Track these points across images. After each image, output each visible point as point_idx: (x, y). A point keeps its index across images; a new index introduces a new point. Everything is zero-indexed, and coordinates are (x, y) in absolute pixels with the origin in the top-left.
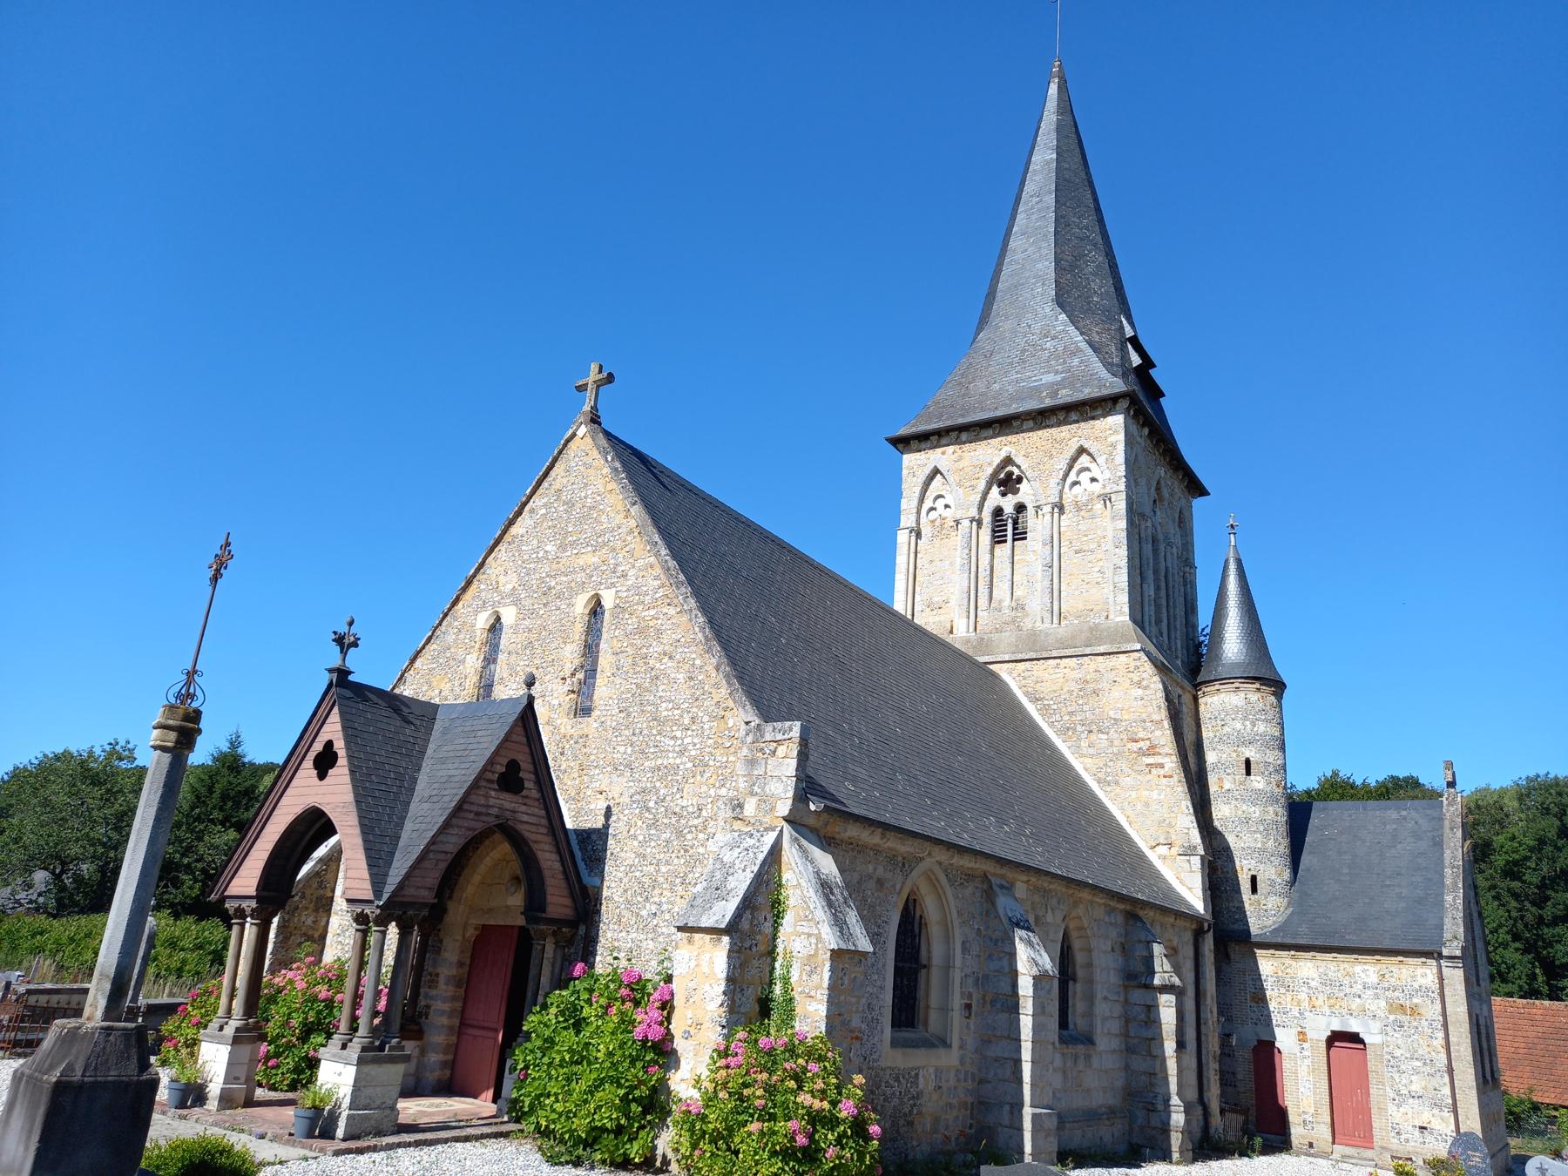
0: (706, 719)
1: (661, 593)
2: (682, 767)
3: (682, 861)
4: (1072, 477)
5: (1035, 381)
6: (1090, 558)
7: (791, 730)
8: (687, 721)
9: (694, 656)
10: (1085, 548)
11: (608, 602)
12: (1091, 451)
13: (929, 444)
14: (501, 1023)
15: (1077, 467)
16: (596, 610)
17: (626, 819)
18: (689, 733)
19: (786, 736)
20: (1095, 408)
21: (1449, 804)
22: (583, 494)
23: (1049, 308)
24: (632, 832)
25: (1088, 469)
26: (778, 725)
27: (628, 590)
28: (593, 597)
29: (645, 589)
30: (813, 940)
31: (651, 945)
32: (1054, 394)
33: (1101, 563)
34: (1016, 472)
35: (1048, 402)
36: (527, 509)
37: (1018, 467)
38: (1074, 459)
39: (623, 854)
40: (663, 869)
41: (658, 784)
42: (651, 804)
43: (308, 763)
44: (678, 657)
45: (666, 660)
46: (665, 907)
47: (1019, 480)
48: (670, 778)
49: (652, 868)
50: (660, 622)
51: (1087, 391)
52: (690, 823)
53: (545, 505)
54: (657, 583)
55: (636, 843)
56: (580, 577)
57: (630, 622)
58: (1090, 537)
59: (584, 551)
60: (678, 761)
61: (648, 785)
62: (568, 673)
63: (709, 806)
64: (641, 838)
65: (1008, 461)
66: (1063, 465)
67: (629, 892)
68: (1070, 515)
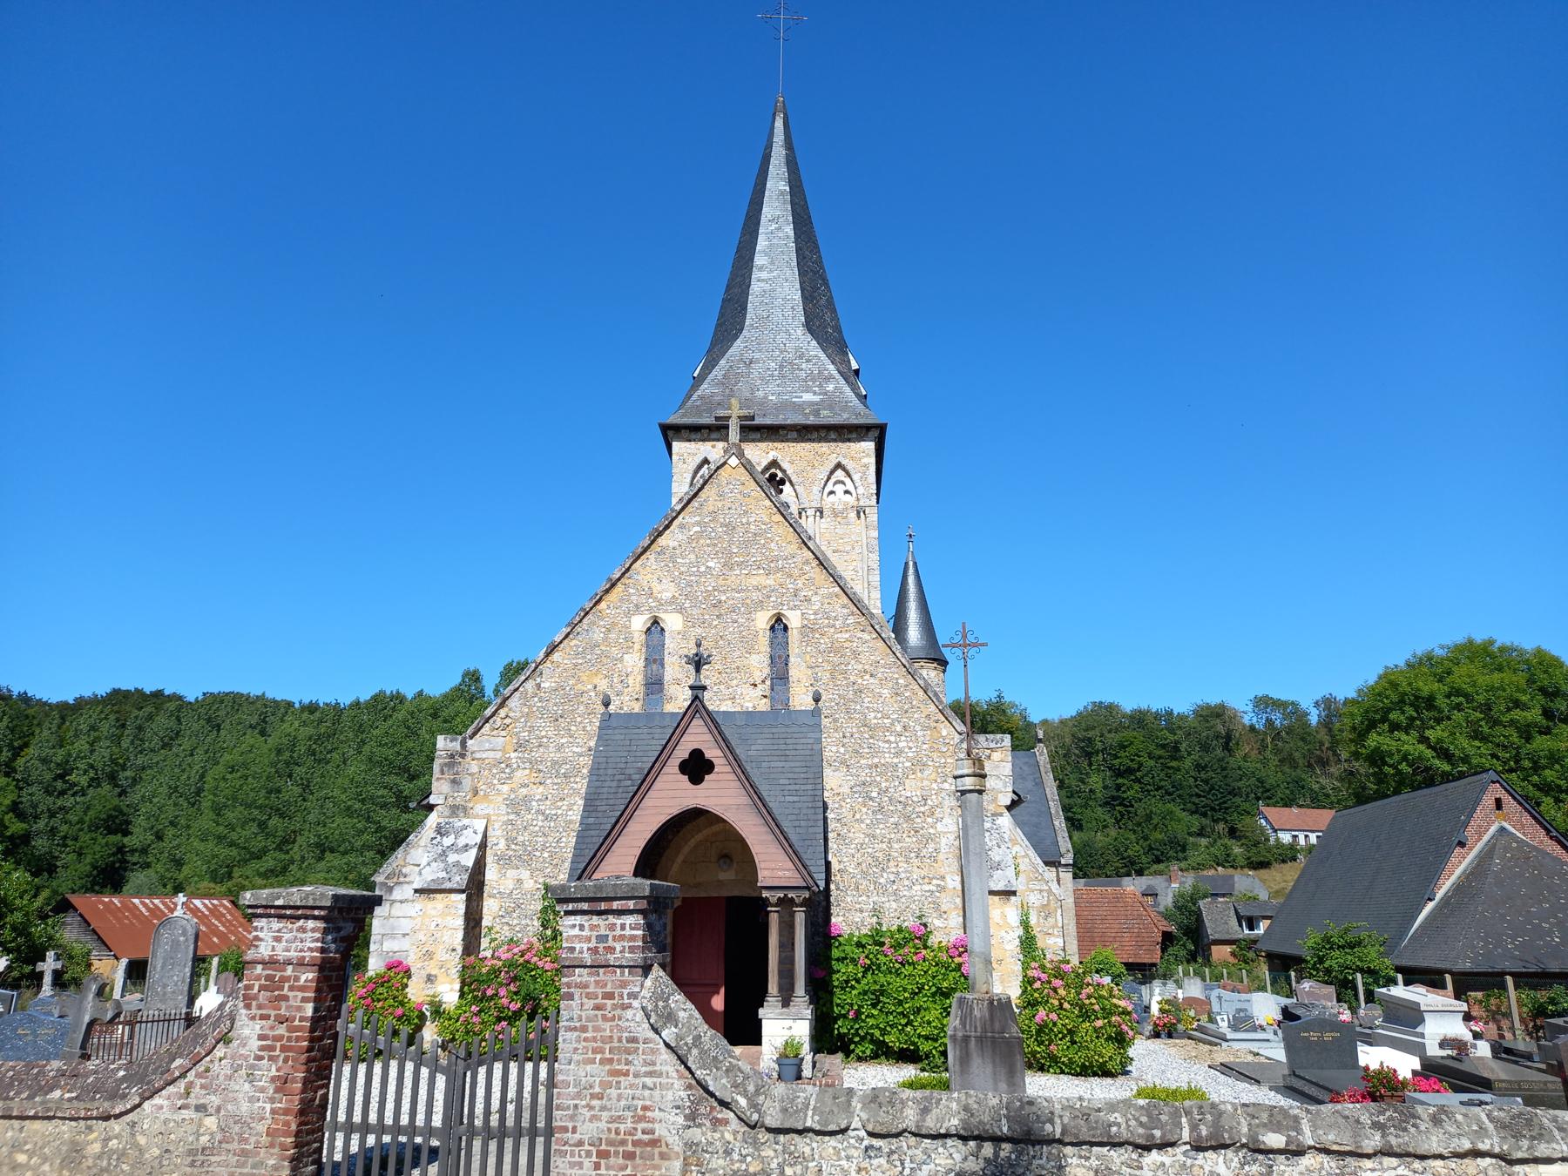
0: (918, 728)
1: (851, 620)
2: (900, 765)
3: (914, 840)
4: (829, 487)
5: (796, 397)
6: (846, 558)
7: (1003, 741)
8: (899, 728)
9: (896, 676)
10: (841, 548)
11: (794, 620)
12: (848, 468)
13: (699, 435)
14: (722, 980)
15: (833, 480)
16: (779, 625)
17: (848, 806)
18: (903, 738)
19: (999, 745)
20: (851, 432)
21: (1040, 755)
22: (744, 520)
23: (800, 331)
24: (858, 816)
25: (843, 483)
26: (991, 736)
27: (815, 614)
28: (774, 615)
29: (834, 614)
30: (1045, 894)
31: (894, 905)
32: (817, 413)
33: (855, 563)
34: (780, 475)
35: (812, 420)
36: (676, 523)
37: (784, 471)
38: (832, 472)
39: (851, 835)
40: (896, 846)
41: (878, 779)
42: (874, 794)
43: (673, 766)
44: (879, 675)
45: (867, 677)
46: (903, 875)
47: (782, 482)
48: (889, 774)
49: (884, 846)
50: (855, 645)
51: (845, 416)
52: (917, 810)
53: (698, 524)
54: (845, 611)
55: (863, 826)
56: (755, 596)
57: (822, 641)
58: (846, 540)
59: (755, 572)
60: (895, 760)
61: (868, 779)
62: (758, 681)
63: (934, 797)
64: (868, 822)
65: (774, 463)
66: (824, 476)
67: (864, 865)
68: (829, 519)
